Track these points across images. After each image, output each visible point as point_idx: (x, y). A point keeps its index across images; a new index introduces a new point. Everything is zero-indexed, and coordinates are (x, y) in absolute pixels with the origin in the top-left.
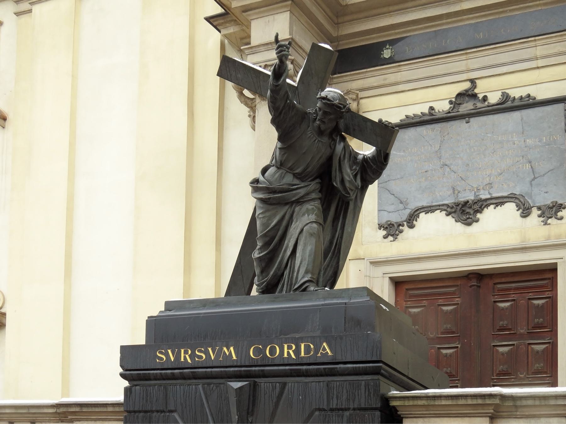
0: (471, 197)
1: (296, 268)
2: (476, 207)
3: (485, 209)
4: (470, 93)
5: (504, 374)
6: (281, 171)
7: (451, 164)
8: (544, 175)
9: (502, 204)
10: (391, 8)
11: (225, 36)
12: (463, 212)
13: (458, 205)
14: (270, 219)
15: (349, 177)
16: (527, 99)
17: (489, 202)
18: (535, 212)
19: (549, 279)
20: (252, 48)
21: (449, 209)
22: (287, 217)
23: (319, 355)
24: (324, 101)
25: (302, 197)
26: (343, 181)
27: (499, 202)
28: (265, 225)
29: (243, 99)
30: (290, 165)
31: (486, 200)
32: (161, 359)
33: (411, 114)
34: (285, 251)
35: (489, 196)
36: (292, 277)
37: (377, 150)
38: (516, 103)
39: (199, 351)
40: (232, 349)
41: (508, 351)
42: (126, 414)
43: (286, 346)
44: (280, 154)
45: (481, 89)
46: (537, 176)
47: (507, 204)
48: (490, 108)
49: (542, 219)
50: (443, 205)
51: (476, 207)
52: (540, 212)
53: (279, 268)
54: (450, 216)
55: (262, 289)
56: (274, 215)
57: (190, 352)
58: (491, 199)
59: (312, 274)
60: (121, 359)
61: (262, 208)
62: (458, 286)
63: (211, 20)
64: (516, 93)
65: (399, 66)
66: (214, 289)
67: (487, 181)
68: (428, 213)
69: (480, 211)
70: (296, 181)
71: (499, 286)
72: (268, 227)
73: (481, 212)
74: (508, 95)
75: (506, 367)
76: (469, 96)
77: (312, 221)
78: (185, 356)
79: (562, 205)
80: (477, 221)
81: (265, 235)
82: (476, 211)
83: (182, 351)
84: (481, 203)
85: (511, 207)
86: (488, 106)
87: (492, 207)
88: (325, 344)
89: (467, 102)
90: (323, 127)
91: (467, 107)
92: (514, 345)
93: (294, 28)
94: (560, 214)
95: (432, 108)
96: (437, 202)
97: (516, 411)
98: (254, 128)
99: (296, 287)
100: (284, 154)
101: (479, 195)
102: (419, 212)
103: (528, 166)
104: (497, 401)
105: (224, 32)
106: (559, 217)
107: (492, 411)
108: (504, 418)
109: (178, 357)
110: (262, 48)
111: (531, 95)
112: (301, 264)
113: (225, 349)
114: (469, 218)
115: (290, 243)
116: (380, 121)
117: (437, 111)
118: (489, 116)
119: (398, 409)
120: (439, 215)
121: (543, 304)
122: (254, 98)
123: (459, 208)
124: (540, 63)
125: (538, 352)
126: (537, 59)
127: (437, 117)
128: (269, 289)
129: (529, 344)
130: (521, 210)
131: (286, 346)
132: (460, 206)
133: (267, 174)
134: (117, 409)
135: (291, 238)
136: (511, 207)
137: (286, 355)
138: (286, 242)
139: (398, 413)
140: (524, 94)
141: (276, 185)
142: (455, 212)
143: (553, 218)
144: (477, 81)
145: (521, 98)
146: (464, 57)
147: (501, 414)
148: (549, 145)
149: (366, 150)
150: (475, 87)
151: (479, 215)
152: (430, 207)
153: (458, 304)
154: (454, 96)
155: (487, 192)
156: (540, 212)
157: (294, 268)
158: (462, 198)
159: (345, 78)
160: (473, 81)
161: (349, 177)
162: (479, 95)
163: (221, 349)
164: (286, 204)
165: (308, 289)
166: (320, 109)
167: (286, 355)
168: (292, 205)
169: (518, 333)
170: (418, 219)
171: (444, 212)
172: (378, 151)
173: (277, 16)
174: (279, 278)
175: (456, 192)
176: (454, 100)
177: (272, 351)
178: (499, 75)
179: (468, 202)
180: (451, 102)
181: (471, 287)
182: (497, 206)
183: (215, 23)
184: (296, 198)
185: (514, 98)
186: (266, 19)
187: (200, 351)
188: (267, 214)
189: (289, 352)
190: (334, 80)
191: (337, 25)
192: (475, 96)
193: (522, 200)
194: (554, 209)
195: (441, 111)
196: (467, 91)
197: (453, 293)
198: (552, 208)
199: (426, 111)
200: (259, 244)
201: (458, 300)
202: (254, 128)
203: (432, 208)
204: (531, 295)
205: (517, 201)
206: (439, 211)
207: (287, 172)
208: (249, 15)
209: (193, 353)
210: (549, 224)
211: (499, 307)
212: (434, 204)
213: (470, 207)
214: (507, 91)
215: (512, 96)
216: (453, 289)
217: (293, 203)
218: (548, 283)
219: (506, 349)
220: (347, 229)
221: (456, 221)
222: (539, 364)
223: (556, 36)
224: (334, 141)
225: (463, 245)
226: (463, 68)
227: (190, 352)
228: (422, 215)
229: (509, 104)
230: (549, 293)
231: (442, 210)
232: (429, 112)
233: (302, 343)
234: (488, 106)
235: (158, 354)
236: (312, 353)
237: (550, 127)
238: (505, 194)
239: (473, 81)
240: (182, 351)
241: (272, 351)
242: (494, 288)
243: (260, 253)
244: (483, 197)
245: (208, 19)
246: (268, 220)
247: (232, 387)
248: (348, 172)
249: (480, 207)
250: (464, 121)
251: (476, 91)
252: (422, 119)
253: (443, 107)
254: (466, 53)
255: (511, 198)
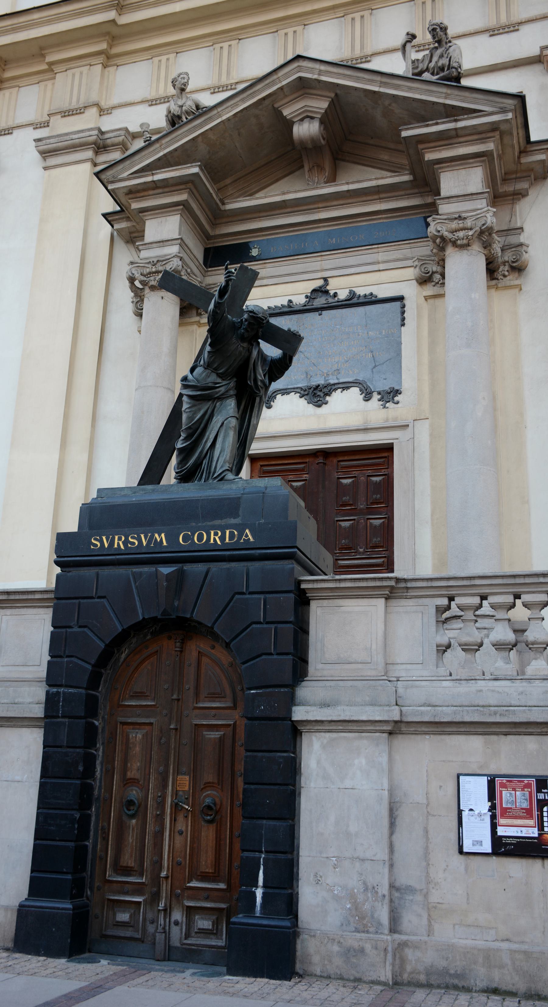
0: (322, 382)
1: (215, 459)
2: (325, 390)
3: (334, 393)
4: (323, 289)
5: (346, 549)
6: (207, 371)
7: (305, 351)
8: (383, 364)
9: (348, 388)
10: (262, 214)
11: (118, 231)
12: (315, 395)
13: (310, 389)
14: (195, 413)
15: (261, 376)
16: (370, 297)
17: (336, 386)
18: (376, 397)
19: (385, 457)
20: (145, 244)
21: (302, 392)
22: (209, 412)
23: (242, 541)
24: (251, 314)
25: (222, 395)
26: (255, 380)
27: (346, 386)
28: (190, 418)
29: (134, 289)
30: (215, 366)
31: (334, 384)
32: (96, 545)
33: (272, 305)
34: (206, 442)
35: (336, 381)
36: (211, 466)
37: (284, 353)
38: (361, 300)
39: (132, 538)
40: (163, 535)
41: (350, 526)
42: (56, 601)
43: (212, 533)
44: (208, 356)
45: (332, 287)
46: (377, 364)
47: (352, 389)
48: (340, 303)
49: (381, 403)
50: (297, 388)
51: (325, 390)
52: (379, 397)
53: (198, 457)
54: (303, 399)
55: (179, 476)
56: (200, 410)
57: (123, 538)
58: (339, 383)
59: (230, 464)
60: (56, 546)
61: (190, 403)
62: (306, 463)
63: (107, 216)
64: (361, 291)
65: (265, 263)
66: (86, 464)
67: (335, 367)
68: (284, 394)
69: (328, 394)
70: (219, 380)
71: (342, 463)
72: (193, 420)
73: (329, 396)
74: (354, 292)
75: (347, 541)
76: (322, 291)
77: (231, 415)
78: (119, 543)
79: (398, 390)
80: (326, 403)
81: (189, 428)
82: (325, 394)
83: (116, 537)
84: (329, 388)
85: (355, 391)
86: (338, 302)
87: (339, 390)
88: (247, 531)
89: (320, 297)
90: (246, 335)
91: (320, 301)
92: (354, 520)
93: (183, 228)
94: (396, 399)
95: (290, 301)
96: (292, 385)
97: (407, 592)
98: (139, 314)
99: (215, 476)
100: (211, 357)
101: (328, 380)
102: (276, 394)
103: (370, 355)
104: (393, 583)
105: (116, 226)
106: (395, 401)
107: (388, 592)
108: (396, 598)
109: (112, 543)
110: (154, 245)
111: (374, 293)
112: (220, 454)
113: (156, 535)
114: (320, 400)
115: (210, 435)
116: (289, 330)
117: (294, 304)
118: (339, 310)
119: (307, 592)
120: (294, 397)
121: (380, 481)
122: (141, 289)
123: (311, 391)
124: (381, 267)
125: (375, 526)
126: (379, 263)
127: (295, 309)
128: (186, 476)
129: (368, 519)
130: (364, 395)
131: (212, 533)
132: (312, 389)
133: (195, 373)
134: (46, 596)
135: (212, 430)
136: (355, 391)
137: (212, 541)
138: (207, 434)
139: (307, 595)
140: (368, 293)
141: (202, 384)
142: (307, 395)
143: (391, 402)
144: (329, 279)
145: (365, 296)
146: (319, 259)
147: (395, 595)
148: (387, 337)
149: (271, 351)
150: (328, 285)
151: (328, 398)
152: (286, 389)
153: (306, 480)
154: (310, 291)
155: (335, 377)
156: (379, 397)
157: (213, 457)
158: (314, 383)
159: (217, 272)
160: (325, 279)
161: (261, 376)
162: (330, 292)
163: (153, 536)
164: (209, 400)
165: (226, 478)
166: (246, 320)
167: (212, 541)
168: (213, 402)
169: (358, 508)
170: (275, 400)
171: (298, 394)
172: (284, 355)
173: (168, 218)
174: (198, 465)
175: (309, 376)
176: (309, 294)
177: (200, 538)
178: (348, 275)
179: (319, 385)
180: (307, 297)
181: (318, 464)
182: (344, 390)
183: (109, 219)
184: (218, 395)
185: (360, 296)
186: (159, 220)
187: (95, 539)
188: (193, 409)
189: (215, 538)
190: (209, 273)
191: (214, 224)
192: (327, 292)
193: (364, 385)
194: (392, 394)
195: (298, 304)
196: (320, 287)
197: (302, 470)
198: (389, 393)
199: (286, 303)
200: (183, 435)
201: (306, 476)
202: (139, 314)
203: (287, 391)
204: (370, 472)
205: (360, 386)
206: (294, 393)
207: (212, 372)
208: (145, 216)
209: (126, 538)
210: (388, 408)
211: (342, 483)
212: (289, 387)
213: (321, 391)
214: (354, 289)
215: (358, 294)
216: (302, 466)
217: (215, 398)
218: (384, 461)
219: (347, 524)
220: (253, 421)
221: (308, 403)
222: (376, 538)
223: (395, 245)
224: (252, 345)
225: (313, 425)
226: (319, 268)
227: (123, 538)
228: (279, 397)
229: (355, 300)
230: (386, 470)
231: (296, 392)
232: (288, 305)
233: (227, 529)
234: (338, 302)
235: (93, 541)
236: (236, 539)
237: (388, 322)
238: (350, 380)
239: (325, 279)
240: (116, 537)
241: (200, 538)
242: (338, 465)
243: (183, 444)
244: (332, 382)
245: (105, 216)
246: (193, 414)
247: (163, 574)
248: (261, 374)
249: (329, 391)
250: (317, 313)
251: (328, 288)
252: (281, 310)
253: (300, 300)
254: (322, 256)
255: (356, 383)
